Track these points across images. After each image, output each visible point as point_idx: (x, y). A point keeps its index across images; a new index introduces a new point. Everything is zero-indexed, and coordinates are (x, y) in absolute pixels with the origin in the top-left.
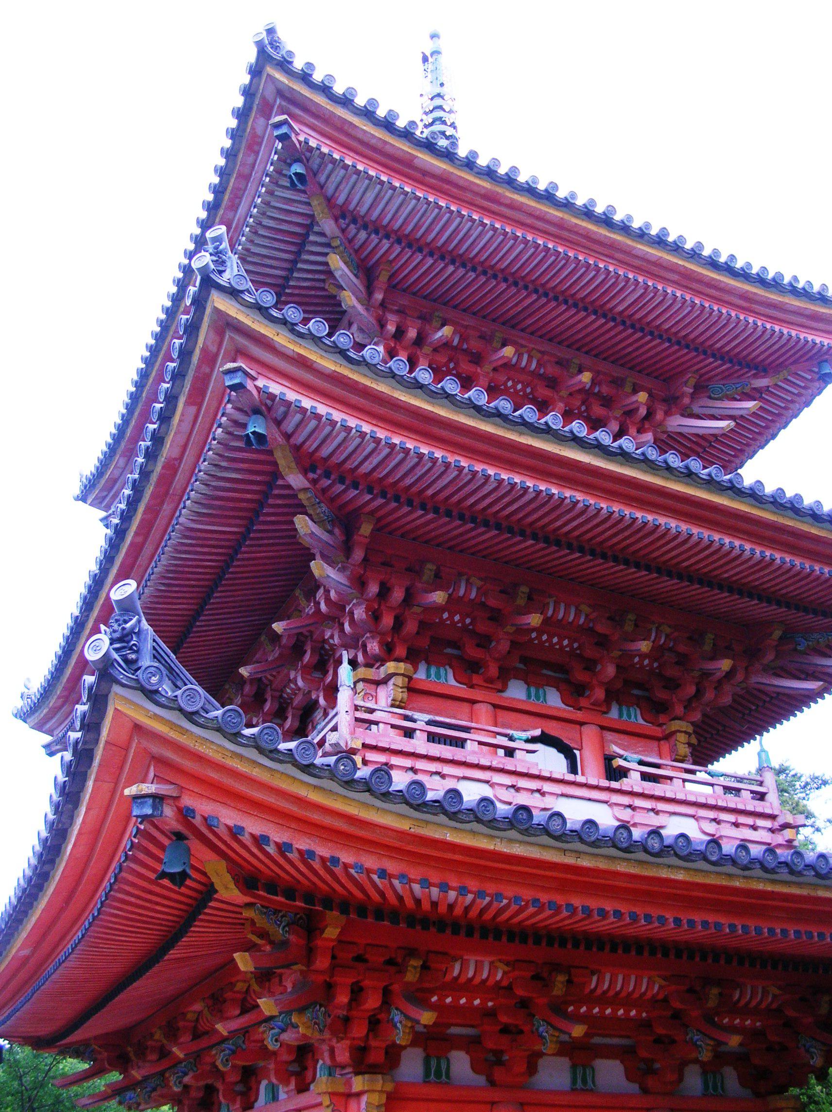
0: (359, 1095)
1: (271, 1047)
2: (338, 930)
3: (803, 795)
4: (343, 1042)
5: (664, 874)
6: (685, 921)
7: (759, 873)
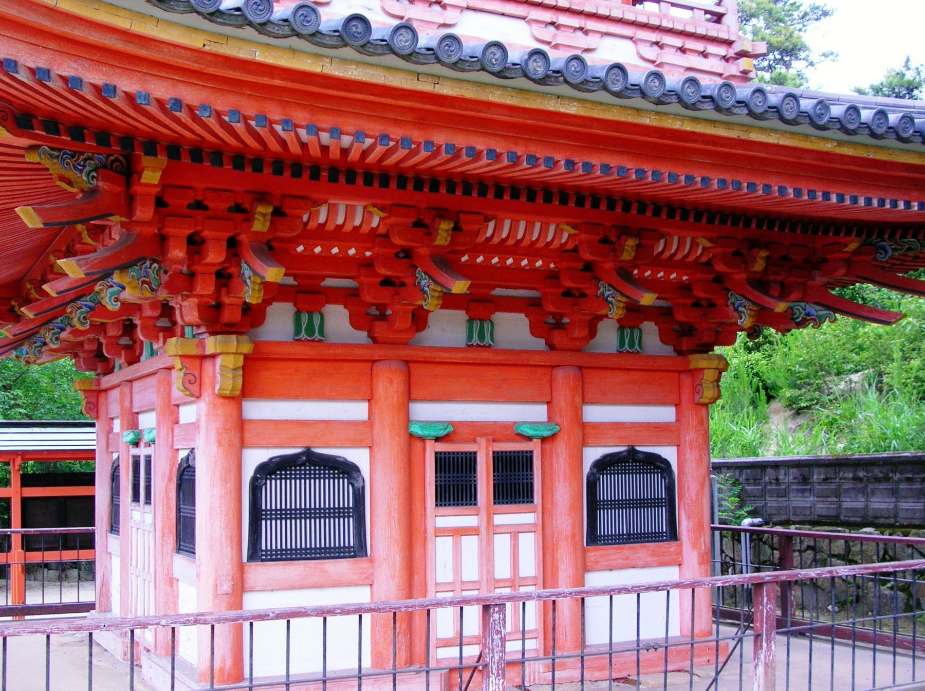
0: (213, 356)
1: (110, 308)
2: (158, 174)
3: (800, 26)
4: (190, 299)
5: (551, 106)
6: (580, 165)
7: (676, 108)
